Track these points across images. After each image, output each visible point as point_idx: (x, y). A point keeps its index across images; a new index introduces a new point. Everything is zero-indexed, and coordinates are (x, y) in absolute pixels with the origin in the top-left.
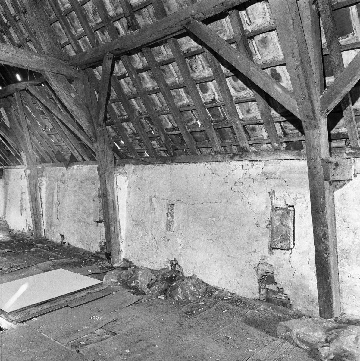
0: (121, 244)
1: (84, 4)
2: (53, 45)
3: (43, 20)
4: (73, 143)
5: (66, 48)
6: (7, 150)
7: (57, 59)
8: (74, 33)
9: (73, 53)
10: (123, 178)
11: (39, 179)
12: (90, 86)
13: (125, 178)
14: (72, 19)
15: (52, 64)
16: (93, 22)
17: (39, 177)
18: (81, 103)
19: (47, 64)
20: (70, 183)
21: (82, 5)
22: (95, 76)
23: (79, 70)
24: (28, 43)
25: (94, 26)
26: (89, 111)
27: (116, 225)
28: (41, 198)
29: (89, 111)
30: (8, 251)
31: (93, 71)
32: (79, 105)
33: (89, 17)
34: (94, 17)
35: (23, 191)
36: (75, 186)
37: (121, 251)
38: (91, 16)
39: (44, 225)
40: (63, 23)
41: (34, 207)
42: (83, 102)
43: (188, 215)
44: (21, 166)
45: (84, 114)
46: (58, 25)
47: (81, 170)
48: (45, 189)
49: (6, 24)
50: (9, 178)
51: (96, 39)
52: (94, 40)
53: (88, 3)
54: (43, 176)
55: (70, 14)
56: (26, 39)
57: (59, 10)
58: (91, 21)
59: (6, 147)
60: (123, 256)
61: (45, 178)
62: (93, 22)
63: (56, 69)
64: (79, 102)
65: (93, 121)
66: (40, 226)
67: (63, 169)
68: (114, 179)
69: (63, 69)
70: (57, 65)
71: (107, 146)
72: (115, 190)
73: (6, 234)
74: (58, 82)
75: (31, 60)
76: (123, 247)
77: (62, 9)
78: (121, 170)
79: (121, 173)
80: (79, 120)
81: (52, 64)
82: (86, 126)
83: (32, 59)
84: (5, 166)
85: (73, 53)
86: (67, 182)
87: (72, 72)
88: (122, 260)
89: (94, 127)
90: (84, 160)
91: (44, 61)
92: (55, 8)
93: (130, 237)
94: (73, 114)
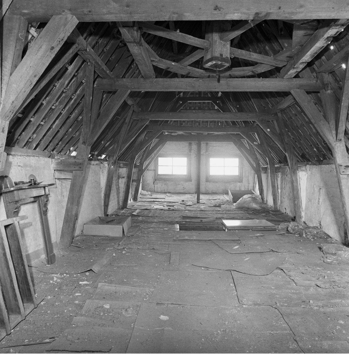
0: (302, 213)
10: (304, 173)
13: (306, 173)
17: (276, 172)
27: (298, 201)
28: (277, 185)
30: (253, 213)
37: (302, 216)
39: (279, 203)
41: (273, 191)
54: (279, 172)
60: (303, 219)
66: (277, 202)
68: (297, 174)
71: (293, 155)
72: (298, 180)
73: (259, 206)
76: (303, 214)
78: (304, 168)
79: (302, 170)
88: (303, 222)
93: (307, 208)
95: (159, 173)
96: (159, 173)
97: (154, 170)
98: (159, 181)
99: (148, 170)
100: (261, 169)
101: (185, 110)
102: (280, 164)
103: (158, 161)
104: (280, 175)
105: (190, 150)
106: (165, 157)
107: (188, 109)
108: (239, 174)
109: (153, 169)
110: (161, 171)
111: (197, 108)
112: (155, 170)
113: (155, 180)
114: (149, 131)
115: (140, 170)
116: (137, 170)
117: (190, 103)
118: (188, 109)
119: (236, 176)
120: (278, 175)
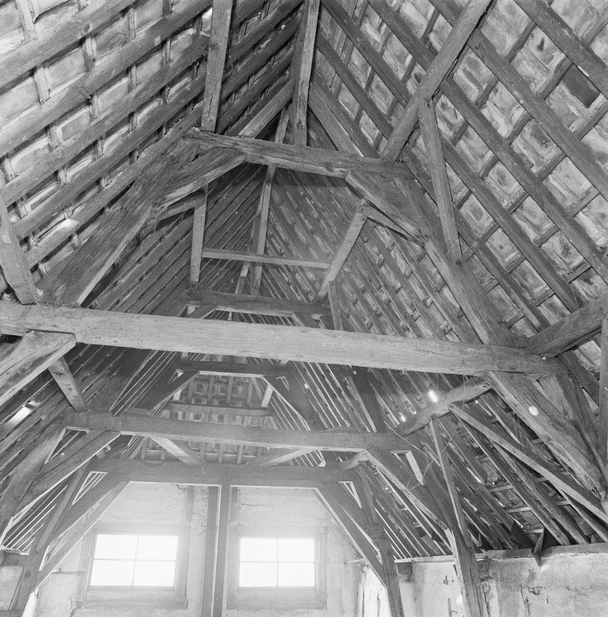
1: (545, 243)
2: (497, 326)
3: (475, 290)
4: (545, 506)
5: (515, 328)
6: (418, 526)
7: (507, 348)
8: (529, 298)
9: (529, 333)
11: (483, 583)
12: (573, 386)
14: (524, 275)
15: (500, 357)
16: (564, 269)
17: (482, 580)
18: (563, 421)
19: (491, 359)
20: (551, 594)
21: (539, 247)
22: (582, 365)
23: (548, 359)
24: (447, 336)
25: (567, 275)
26: (582, 436)
29: (582, 436)
31: (575, 355)
32: (561, 425)
33: (554, 263)
34: (565, 259)
35: (452, 609)
36: (565, 603)
38: (558, 261)
40: (508, 286)
42: (565, 418)
43: (388, 575)
44: (443, 556)
45: (574, 442)
46: (499, 292)
47: (572, 565)
48: (498, 607)
49: (412, 316)
50: (423, 581)
51: (576, 295)
52: (573, 298)
53: (551, 240)
54: (489, 578)
55: (519, 268)
56: (444, 331)
57: (499, 267)
58: (559, 268)
59: (416, 521)
61: (494, 581)
62: (564, 269)
63: (507, 365)
64: (559, 419)
65: (593, 455)
67: (531, 561)
69: (519, 362)
70: (507, 358)
74: (515, 387)
75: (464, 356)
77: (503, 264)
80: (565, 456)
81: (500, 357)
82: (583, 466)
83: (466, 355)
84: (414, 557)
85: (529, 333)
86: (543, 591)
87: (534, 364)
89: (599, 468)
90: (573, 542)
91: (486, 355)
92: (491, 266)
94: (552, 444)
95: (92, 584)
96: (92, 584)
97: (79, 573)
98: (92, 607)
99: (60, 572)
100: (397, 570)
101: (183, 404)
102: (486, 550)
103: (94, 544)
104: (493, 587)
105: (190, 514)
106: (114, 533)
107: (193, 402)
108: (316, 583)
109: (76, 570)
110: (100, 577)
111: (216, 402)
112: (83, 574)
113: (79, 605)
114: (73, 432)
115: (27, 575)
116: (18, 575)
117: (207, 379)
118: (193, 402)
119: (307, 589)
120: (487, 589)
